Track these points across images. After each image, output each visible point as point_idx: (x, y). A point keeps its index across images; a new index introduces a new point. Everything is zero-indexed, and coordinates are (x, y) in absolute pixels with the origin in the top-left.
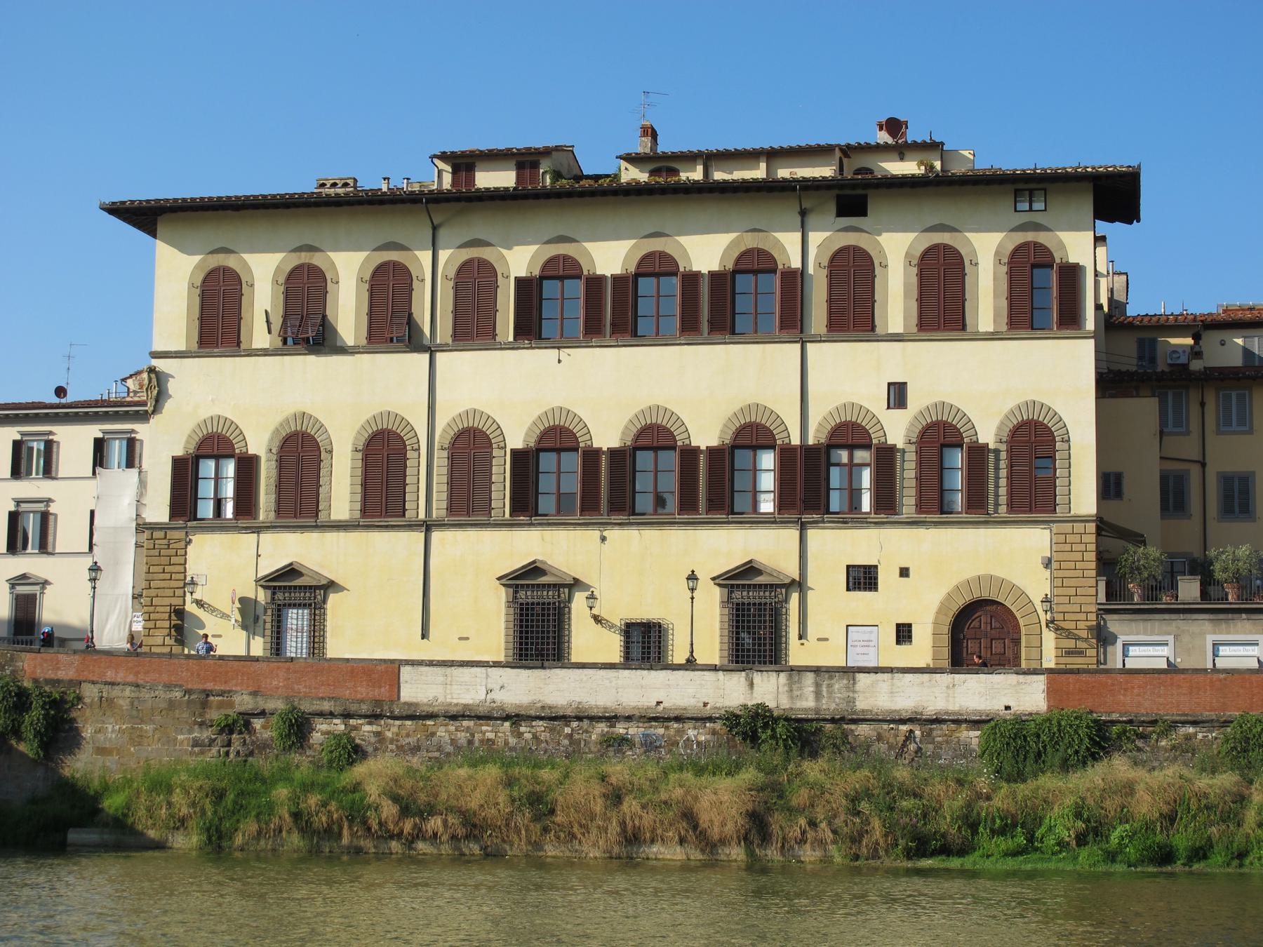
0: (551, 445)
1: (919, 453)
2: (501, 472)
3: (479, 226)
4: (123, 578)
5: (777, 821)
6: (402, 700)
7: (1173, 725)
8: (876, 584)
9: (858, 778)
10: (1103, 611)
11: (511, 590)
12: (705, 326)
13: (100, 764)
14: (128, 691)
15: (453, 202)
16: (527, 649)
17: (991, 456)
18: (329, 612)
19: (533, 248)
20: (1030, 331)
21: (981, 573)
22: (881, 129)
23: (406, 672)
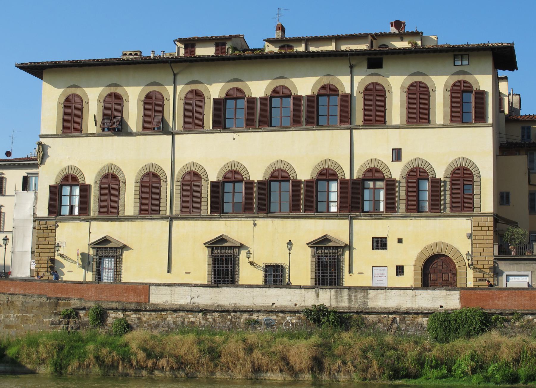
0: (230, 179)
1: (407, 183)
2: (206, 193)
3: (196, 74)
4: (26, 243)
5: (327, 361)
6: (151, 302)
7: (522, 315)
8: (386, 246)
9: (367, 341)
10: (497, 260)
11: (211, 249)
12: (304, 122)
13: (7, 333)
14: (21, 298)
15: (185, 62)
16: (218, 278)
17: (442, 184)
18: (123, 260)
19: (222, 84)
20: (461, 124)
21: (437, 241)
22: (392, 26)
23: (152, 288)
